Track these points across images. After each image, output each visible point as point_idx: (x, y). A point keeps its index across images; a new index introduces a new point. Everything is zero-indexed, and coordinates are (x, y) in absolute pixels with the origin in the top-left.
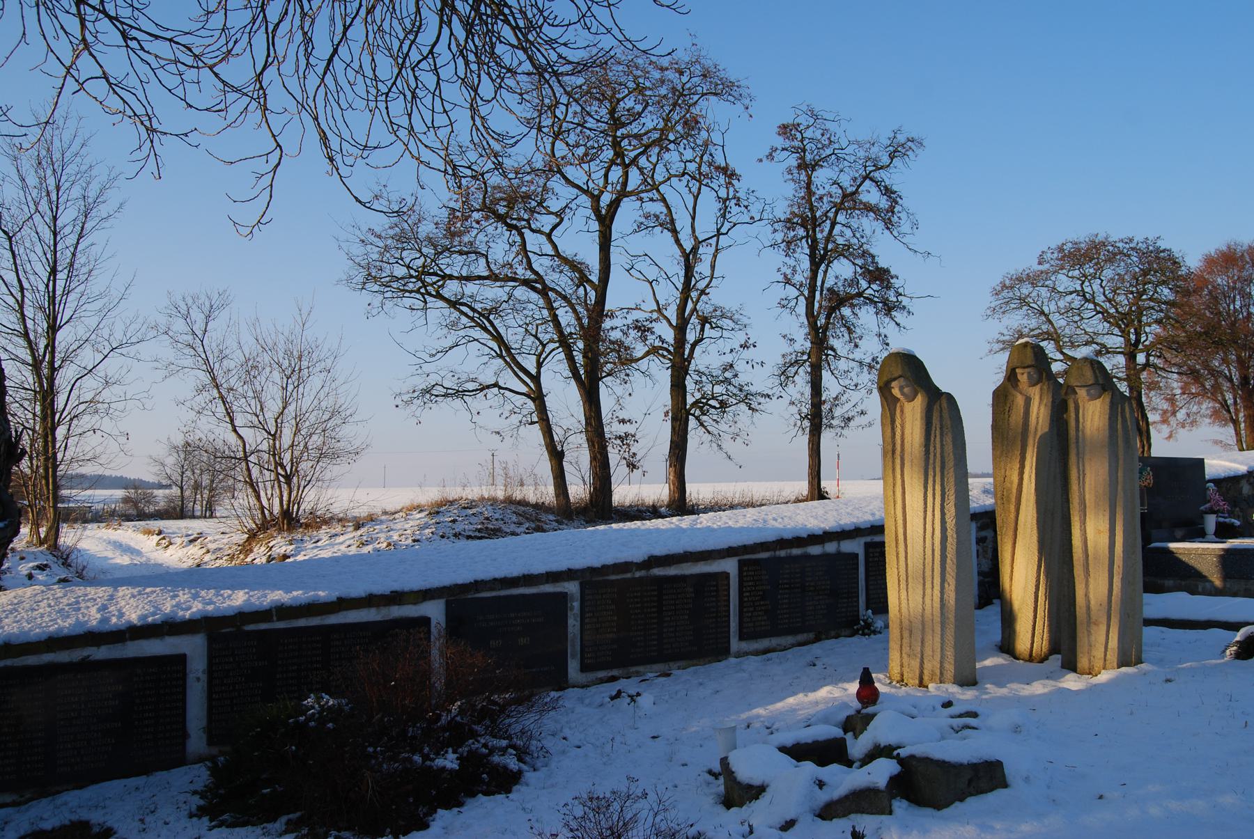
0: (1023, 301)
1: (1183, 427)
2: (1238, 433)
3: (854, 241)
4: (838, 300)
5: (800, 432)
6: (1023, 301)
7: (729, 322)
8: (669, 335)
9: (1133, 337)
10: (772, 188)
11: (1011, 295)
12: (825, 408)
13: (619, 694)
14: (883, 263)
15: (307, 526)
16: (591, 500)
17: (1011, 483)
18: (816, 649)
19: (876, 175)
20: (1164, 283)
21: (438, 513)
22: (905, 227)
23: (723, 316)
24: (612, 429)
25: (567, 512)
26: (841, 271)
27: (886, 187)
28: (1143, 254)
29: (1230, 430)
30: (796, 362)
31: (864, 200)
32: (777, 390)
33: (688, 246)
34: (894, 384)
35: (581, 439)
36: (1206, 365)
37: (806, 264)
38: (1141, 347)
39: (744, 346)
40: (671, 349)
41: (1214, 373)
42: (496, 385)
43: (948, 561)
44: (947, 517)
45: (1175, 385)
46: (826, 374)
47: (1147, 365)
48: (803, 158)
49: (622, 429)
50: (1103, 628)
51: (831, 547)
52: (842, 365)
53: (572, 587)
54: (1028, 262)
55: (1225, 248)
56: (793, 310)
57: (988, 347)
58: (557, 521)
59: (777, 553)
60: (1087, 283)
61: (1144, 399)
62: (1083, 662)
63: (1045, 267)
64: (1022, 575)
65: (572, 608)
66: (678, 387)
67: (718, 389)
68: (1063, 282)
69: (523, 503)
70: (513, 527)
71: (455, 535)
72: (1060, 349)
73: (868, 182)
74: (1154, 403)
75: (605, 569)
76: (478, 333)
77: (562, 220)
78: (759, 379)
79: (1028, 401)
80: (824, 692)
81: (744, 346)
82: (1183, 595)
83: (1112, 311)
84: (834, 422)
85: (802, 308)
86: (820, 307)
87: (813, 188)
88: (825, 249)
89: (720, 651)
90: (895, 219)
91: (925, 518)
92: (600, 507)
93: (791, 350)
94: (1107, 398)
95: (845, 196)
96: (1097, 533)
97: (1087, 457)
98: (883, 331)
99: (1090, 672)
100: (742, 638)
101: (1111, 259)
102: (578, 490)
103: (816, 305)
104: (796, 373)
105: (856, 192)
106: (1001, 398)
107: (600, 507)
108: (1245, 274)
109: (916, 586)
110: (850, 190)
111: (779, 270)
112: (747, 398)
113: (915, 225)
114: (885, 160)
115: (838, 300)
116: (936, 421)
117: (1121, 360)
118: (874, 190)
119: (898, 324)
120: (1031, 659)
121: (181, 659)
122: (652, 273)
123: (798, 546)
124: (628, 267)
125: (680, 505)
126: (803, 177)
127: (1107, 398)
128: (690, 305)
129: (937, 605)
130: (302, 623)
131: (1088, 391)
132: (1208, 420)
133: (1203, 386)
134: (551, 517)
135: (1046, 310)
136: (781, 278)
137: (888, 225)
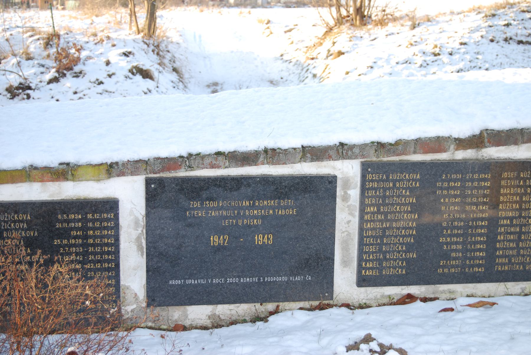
15: (382, 23)
21: (494, 15)
65: (346, 198)
71: (506, 40)
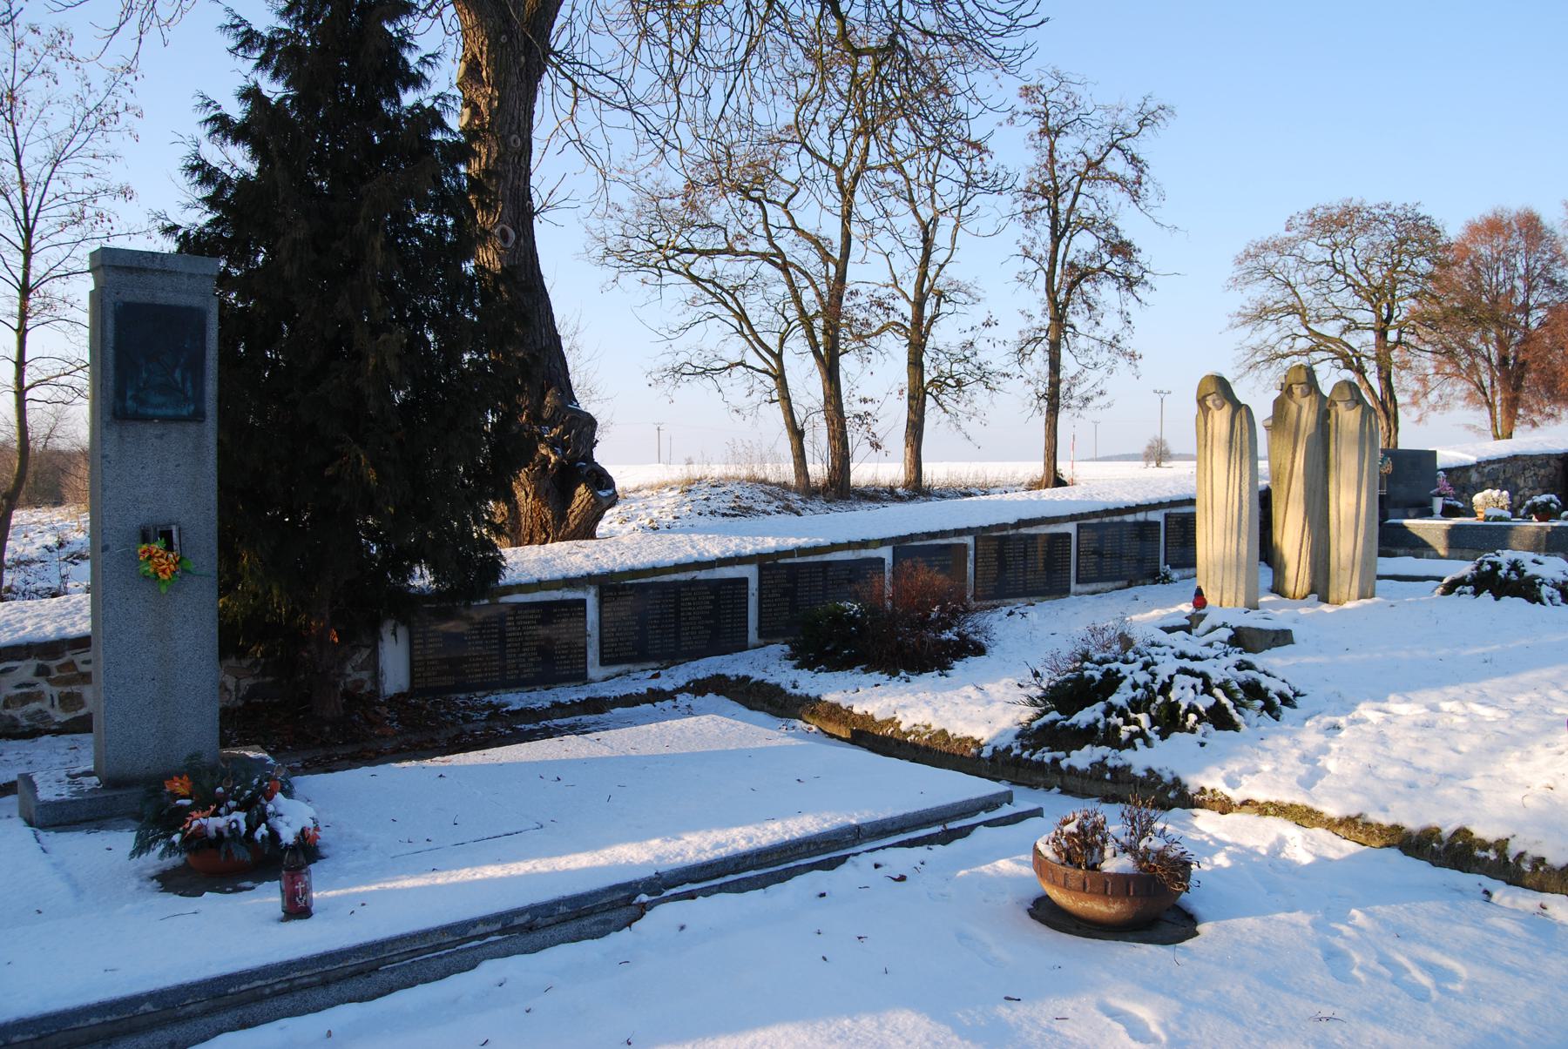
0: (1268, 272)
1: (1434, 409)
2: (1493, 418)
3: (1099, 214)
4: (1080, 274)
5: (1037, 413)
6: (1268, 272)
7: (964, 296)
8: (908, 311)
9: (1385, 311)
10: (1014, 152)
11: (1255, 264)
12: (1063, 387)
13: (1011, 613)
14: (1126, 237)
18: (1133, 591)
19: (1123, 143)
20: (1421, 254)
22: (1152, 200)
23: (958, 290)
24: (851, 407)
25: (809, 491)
26: (1083, 244)
28: (1399, 222)
29: (1485, 412)
31: (1109, 169)
32: (1016, 369)
36: (1463, 343)
38: (1393, 323)
40: (908, 325)
41: (1471, 351)
42: (741, 363)
45: (1428, 364)
46: (1064, 352)
47: (1398, 343)
48: (1045, 123)
49: (860, 408)
51: (1140, 517)
52: (1082, 342)
53: (969, 540)
54: (1275, 229)
55: (1490, 215)
56: (1030, 284)
57: (1228, 321)
60: (1337, 253)
61: (1393, 379)
62: (1333, 596)
63: (1294, 233)
64: (1291, 536)
66: (916, 364)
68: (1313, 251)
69: (764, 482)
70: (763, 506)
72: (1305, 324)
74: (1404, 384)
75: (991, 528)
76: (719, 309)
77: (798, 190)
78: (996, 357)
79: (1300, 408)
80: (1155, 613)
81: (987, 325)
82: (1411, 559)
83: (1364, 284)
84: (1072, 402)
87: (1056, 155)
88: (1067, 220)
89: (1064, 592)
90: (1142, 192)
92: (839, 489)
94: (1359, 409)
96: (1349, 502)
98: (1125, 308)
99: (1338, 603)
100: (1078, 582)
101: (1364, 228)
102: (818, 470)
103: (1057, 280)
106: (1279, 405)
107: (839, 489)
108: (1511, 243)
109: (1218, 540)
112: (984, 377)
114: (1134, 127)
115: (1080, 274)
117: (1371, 337)
121: (745, 581)
125: (917, 489)
126: (1046, 142)
127: (1359, 409)
128: (927, 284)
130: (810, 559)
132: (1461, 403)
133: (1458, 366)
135: (1292, 280)
137: (1135, 197)
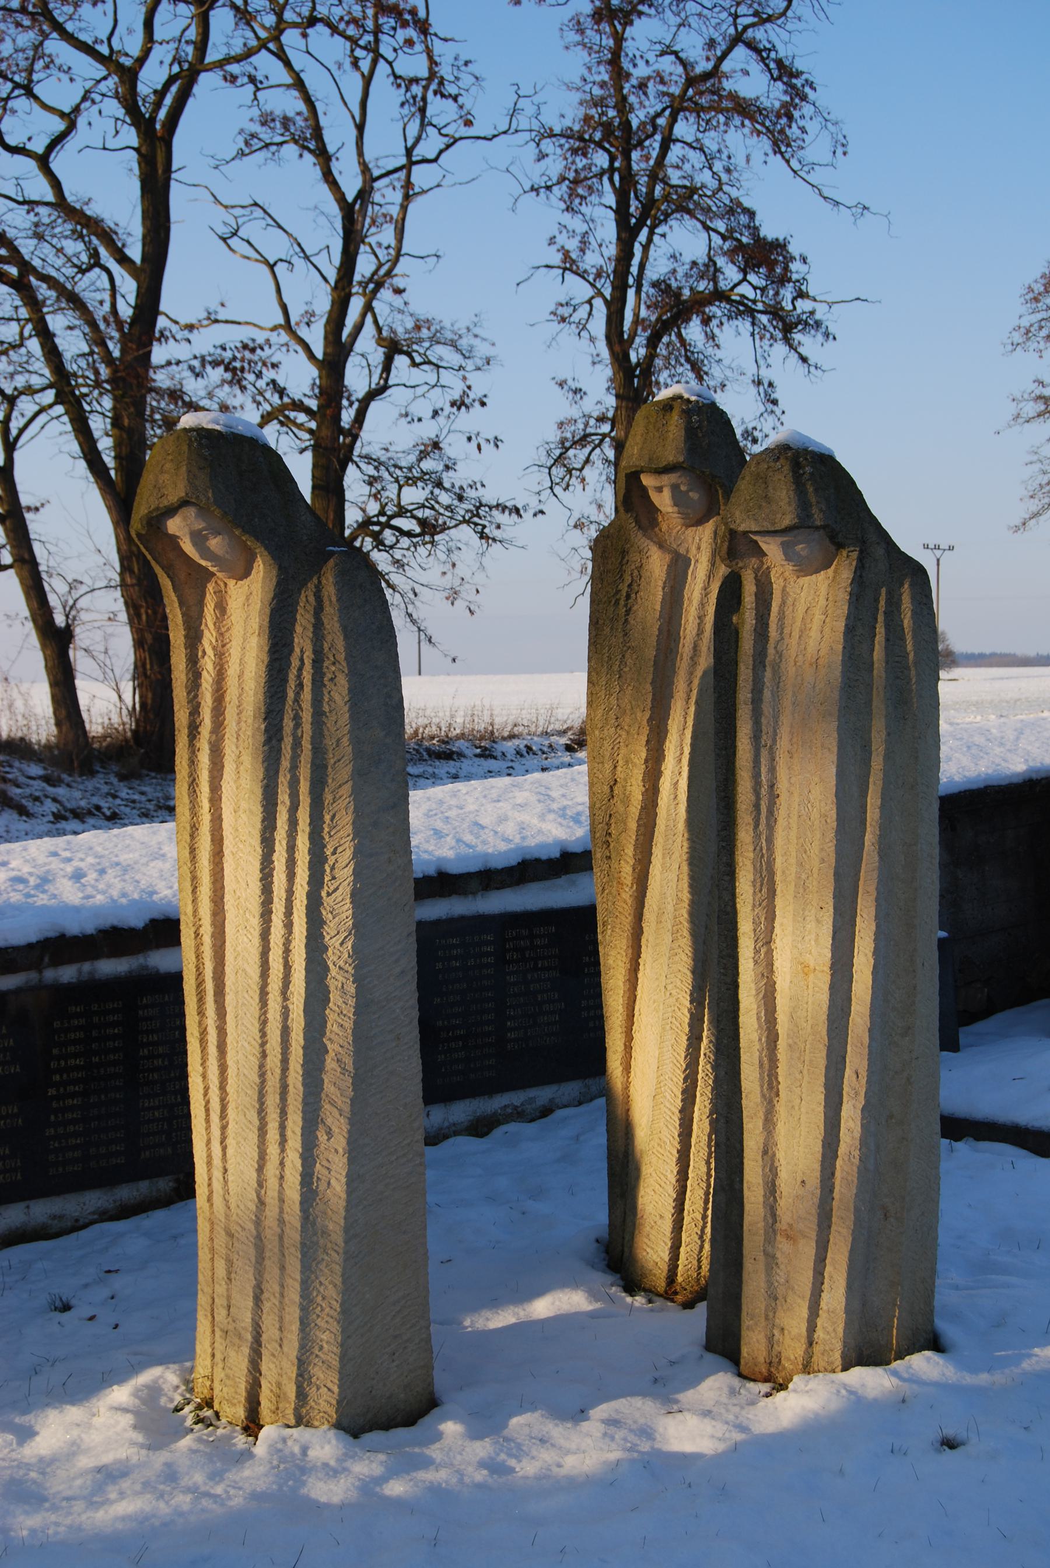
3: (705, 178)
4: (677, 308)
14: (769, 231)
16: (135, 733)
17: (626, 801)
19: (758, 34)
23: (435, 340)
26: (680, 246)
27: (779, 63)
30: (585, 436)
33: (351, 186)
34: (174, 525)
35: (114, 602)
37: (607, 230)
39: (459, 404)
43: (330, 1063)
44: (329, 930)
50: (808, 1249)
56: (582, 327)
57: (1012, 409)
58: (47, 779)
59: (50, 975)
62: (753, 1345)
67: (412, 495)
73: (740, 52)
77: (72, 126)
79: (679, 567)
85: (599, 325)
86: (637, 321)
87: (626, 64)
90: (794, 132)
91: (265, 935)
93: (574, 412)
95: (691, 81)
97: (783, 744)
98: (766, 374)
104: (587, 461)
105: (714, 73)
110: (703, 66)
111: (552, 241)
113: (841, 146)
115: (677, 308)
116: (302, 641)
118: (755, 67)
119: (804, 360)
120: (669, 1293)
122: (275, 246)
123: (117, 951)
124: (225, 231)
129: (293, 1193)
131: (786, 547)
134: (35, 770)
136: (557, 259)
137: (780, 143)
